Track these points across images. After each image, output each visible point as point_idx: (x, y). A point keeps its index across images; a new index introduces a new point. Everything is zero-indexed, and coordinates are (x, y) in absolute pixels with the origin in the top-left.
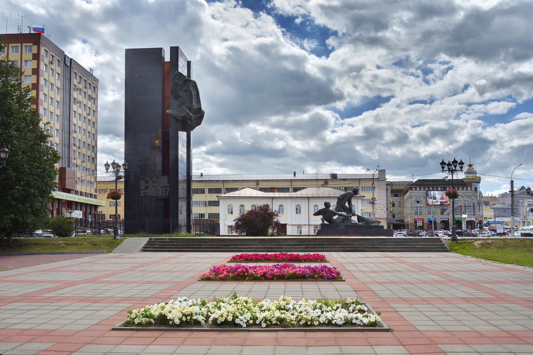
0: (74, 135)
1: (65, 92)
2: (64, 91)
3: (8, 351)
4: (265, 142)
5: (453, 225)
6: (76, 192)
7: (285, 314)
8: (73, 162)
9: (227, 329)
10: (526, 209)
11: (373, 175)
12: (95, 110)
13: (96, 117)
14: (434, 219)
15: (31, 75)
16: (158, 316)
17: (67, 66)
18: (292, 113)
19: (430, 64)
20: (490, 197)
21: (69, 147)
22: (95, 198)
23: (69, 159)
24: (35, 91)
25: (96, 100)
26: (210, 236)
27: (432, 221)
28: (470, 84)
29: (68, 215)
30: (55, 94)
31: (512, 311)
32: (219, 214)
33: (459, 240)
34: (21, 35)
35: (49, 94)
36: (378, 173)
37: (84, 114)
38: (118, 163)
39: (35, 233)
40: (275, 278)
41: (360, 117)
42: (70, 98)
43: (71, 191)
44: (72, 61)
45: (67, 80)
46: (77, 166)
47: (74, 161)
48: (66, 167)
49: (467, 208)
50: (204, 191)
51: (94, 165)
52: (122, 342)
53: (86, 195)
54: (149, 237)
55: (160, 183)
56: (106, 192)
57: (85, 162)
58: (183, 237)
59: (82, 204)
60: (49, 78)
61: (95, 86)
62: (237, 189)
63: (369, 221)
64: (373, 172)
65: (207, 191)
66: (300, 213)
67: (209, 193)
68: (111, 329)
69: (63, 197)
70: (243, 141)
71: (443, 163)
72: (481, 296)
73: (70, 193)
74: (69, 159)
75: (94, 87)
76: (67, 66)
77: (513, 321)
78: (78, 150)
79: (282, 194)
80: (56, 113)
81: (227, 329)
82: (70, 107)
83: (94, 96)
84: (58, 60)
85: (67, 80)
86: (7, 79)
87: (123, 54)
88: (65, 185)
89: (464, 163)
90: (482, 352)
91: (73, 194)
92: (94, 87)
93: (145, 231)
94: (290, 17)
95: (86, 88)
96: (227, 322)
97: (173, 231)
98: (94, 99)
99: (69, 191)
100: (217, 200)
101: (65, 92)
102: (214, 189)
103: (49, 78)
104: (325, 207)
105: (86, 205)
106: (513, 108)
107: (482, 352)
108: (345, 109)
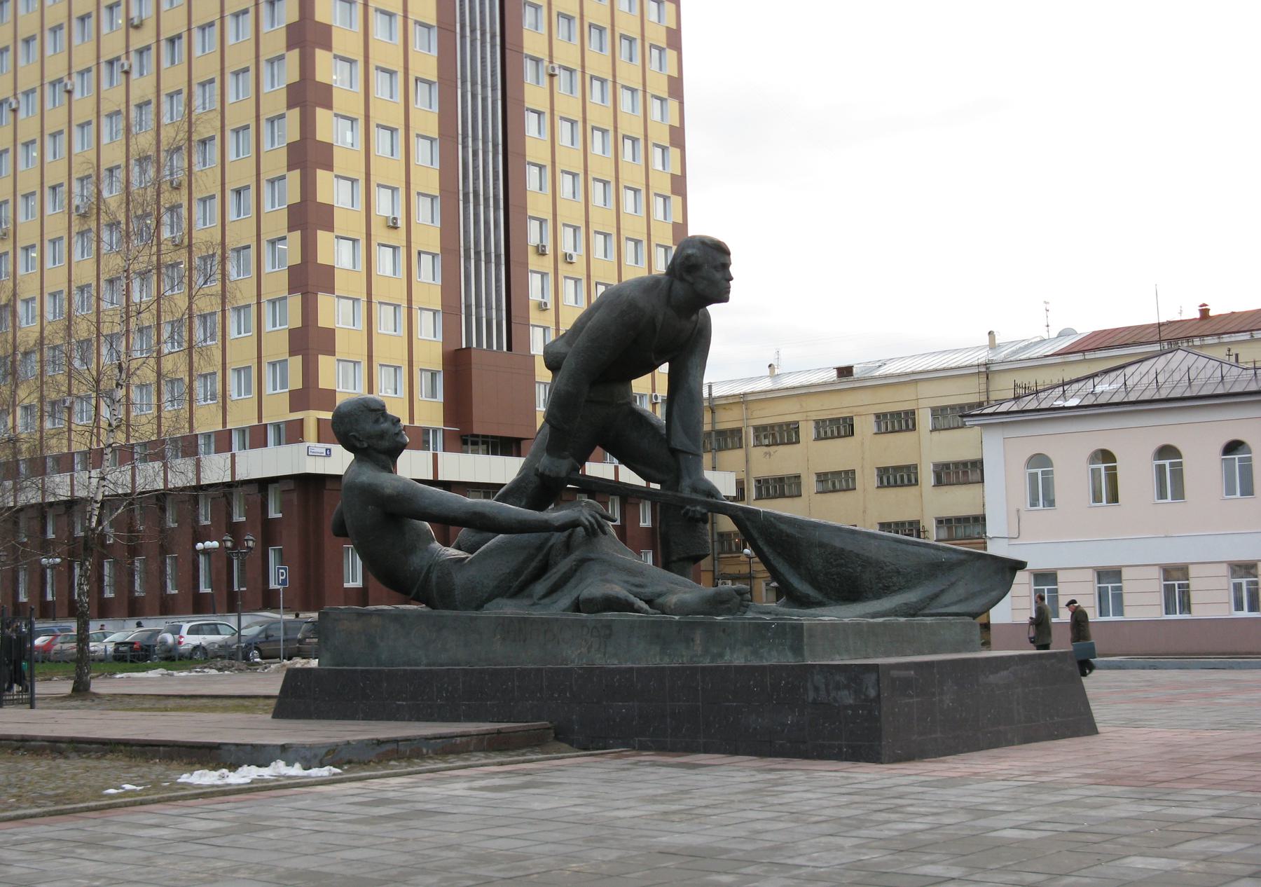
3: (787, 843)
4: (912, 672)
5: (108, 503)
15: (286, 294)
19: (390, 411)
26: (1248, 596)
28: (875, 481)
31: (359, 847)
32: (266, 446)
36: (91, 644)
38: (1204, 312)
39: (9, 565)
48: (469, 348)
49: (1253, 371)
50: (759, 489)
54: (1054, 655)
58: (348, 665)
63: (551, 405)
64: (99, 686)
66: (1179, 494)
71: (1074, 602)
72: (50, 834)
79: (490, 100)
80: (618, 31)
83: (472, 748)
94: (916, 602)
96: (679, 287)
102: (892, 414)
106: (1034, 616)
108: (676, 604)
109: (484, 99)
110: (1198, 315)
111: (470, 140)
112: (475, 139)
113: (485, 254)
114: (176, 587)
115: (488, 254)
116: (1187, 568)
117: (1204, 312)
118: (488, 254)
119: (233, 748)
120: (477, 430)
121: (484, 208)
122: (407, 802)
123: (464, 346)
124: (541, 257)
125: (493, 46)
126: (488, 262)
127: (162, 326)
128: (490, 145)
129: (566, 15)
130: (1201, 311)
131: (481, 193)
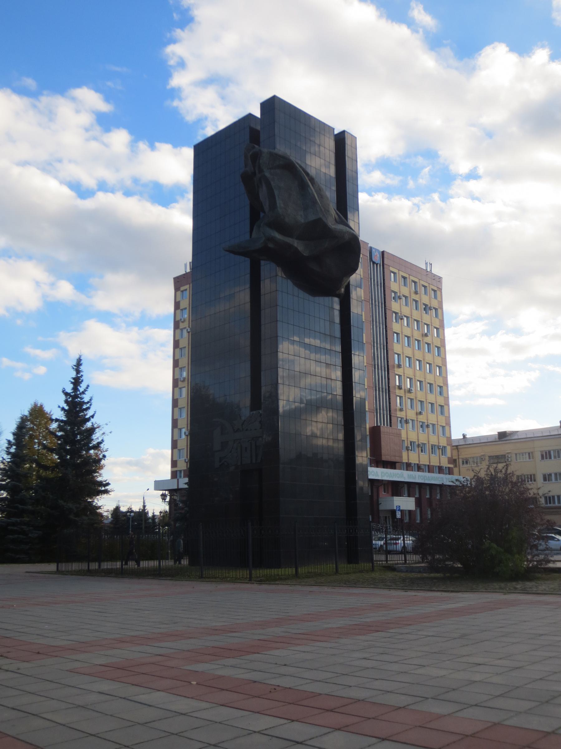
0: (399, 371)
1: (375, 305)
2: (372, 304)
6: (409, 466)
7: (229, 578)
8: (398, 416)
9: (548, 455)
10: (540, 550)
11: (418, 398)
12: (442, 385)
13: (446, 414)
14: (103, 447)
15: (177, 479)
16: (29, 414)
17: (377, 264)
18: (397, 197)
20: (164, 559)
21: (389, 391)
22: (429, 472)
23: (390, 411)
24: (174, 418)
25: (439, 310)
27: (558, 458)
29: (83, 429)
30: (413, 349)
33: (473, 466)
34: (345, 425)
35: (402, 332)
37: (417, 335)
38: (464, 436)
40: (500, 457)
41: (359, 267)
42: (385, 314)
43: (397, 464)
44: (385, 256)
45: (378, 285)
46: (407, 422)
47: (399, 414)
48: (380, 426)
51: (444, 418)
52: (351, 703)
53: (430, 469)
55: (247, 430)
56: (483, 462)
57: (404, 409)
59: (410, 485)
60: (421, 317)
61: (436, 289)
62: (479, 590)
65: (175, 469)
67: (258, 143)
68: (146, 504)
69: (378, 475)
70: (548, 535)
72: (416, 426)
73: (395, 468)
74: (390, 411)
75: (435, 291)
76: (377, 264)
77: (466, 706)
78: (408, 395)
81: (548, 455)
82: (386, 327)
83: (434, 304)
84: (433, 290)
85: (378, 285)
86: (338, 296)
87: (178, 466)
88: (381, 455)
89: (80, 356)
90: (169, 735)
91: (400, 469)
92: (435, 291)
93: (195, 308)
95: (416, 293)
97: (348, 232)
98: (436, 309)
99: (392, 465)
100: (439, 327)
101: (375, 305)
103: (421, 317)
104: (262, 262)
105: (420, 485)
107: (169, 735)
109: (380, 328)
110: (462, 437)
111: (383, 371)
112: (377, 344)
113: (382, 389)
114: (132, 532)
115: (382, 389)
116: (408, 496)
117: (464, 436)
118: (382, 389)
119: (447, 486)
120: (384, 458)
121: (378, 392)
122: (391, 643)
123: (376, 425)
124: (400, 390)
125: (382, 308)
126: (383, 392)
127: (186, 427)
128: (382, 346)
129: (414, 281)
130: (463, 436)
131: (377, 386)
